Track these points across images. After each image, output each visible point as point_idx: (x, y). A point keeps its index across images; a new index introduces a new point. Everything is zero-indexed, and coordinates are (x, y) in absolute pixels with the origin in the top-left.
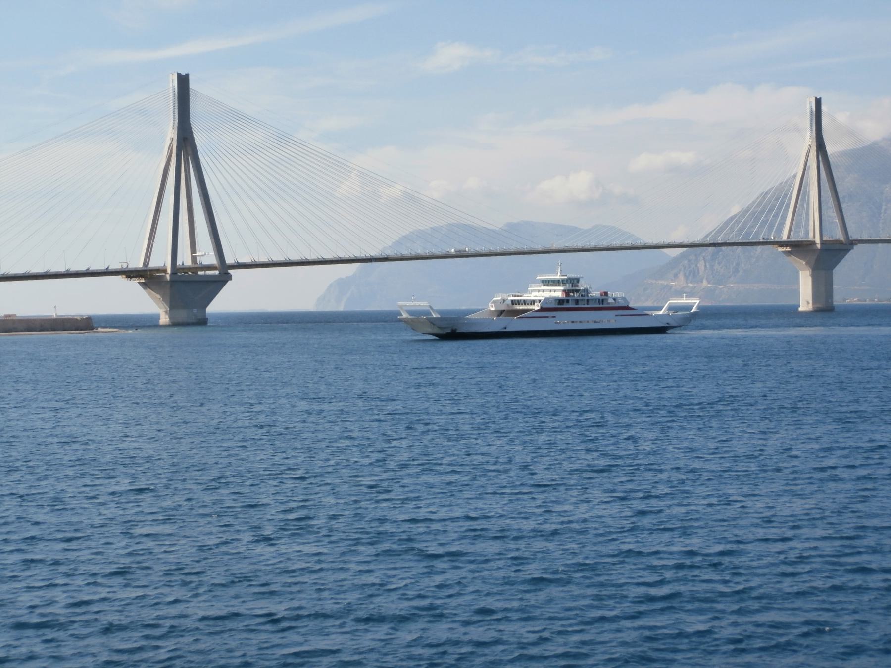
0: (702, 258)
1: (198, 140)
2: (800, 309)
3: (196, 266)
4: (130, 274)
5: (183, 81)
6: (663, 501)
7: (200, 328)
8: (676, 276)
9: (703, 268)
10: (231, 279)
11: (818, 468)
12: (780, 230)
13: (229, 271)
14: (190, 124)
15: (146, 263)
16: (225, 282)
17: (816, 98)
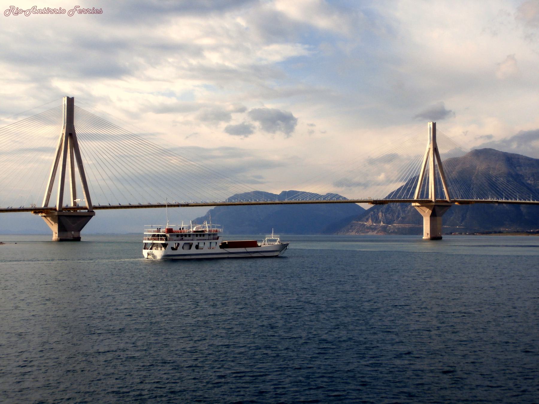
0: (380, 211)
1: (412, 175)
3: (76, 207)
4: (37, 211)
5: (71, 101)
7: (76, 243)
9: (381, 216)
10: (172, 229)
11: (49, 241)
13: (94, 210)
14: (74, 126)
15: (46, 205)
16: (91, 217)
17: (68, 98)
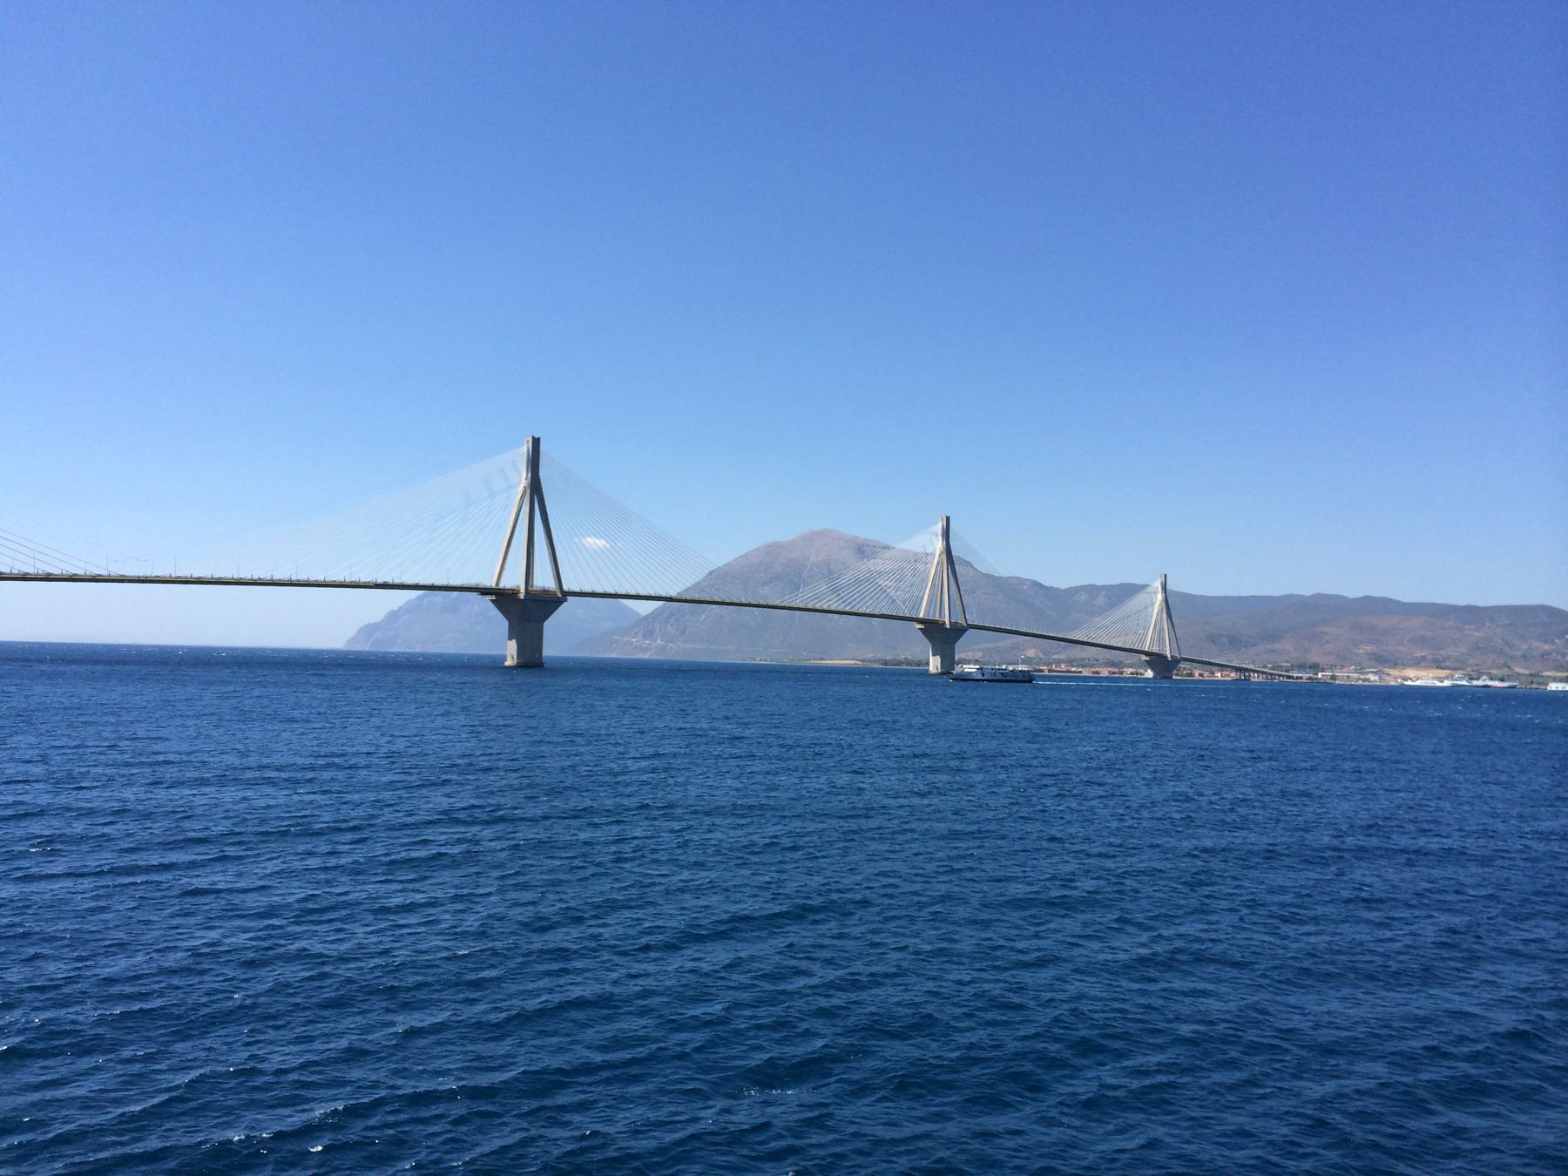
2: (507, 664)
4: (484, 591)
6: (792, 983)
8: (637, 633)
12: (918, 610)
15: (497, 584)
